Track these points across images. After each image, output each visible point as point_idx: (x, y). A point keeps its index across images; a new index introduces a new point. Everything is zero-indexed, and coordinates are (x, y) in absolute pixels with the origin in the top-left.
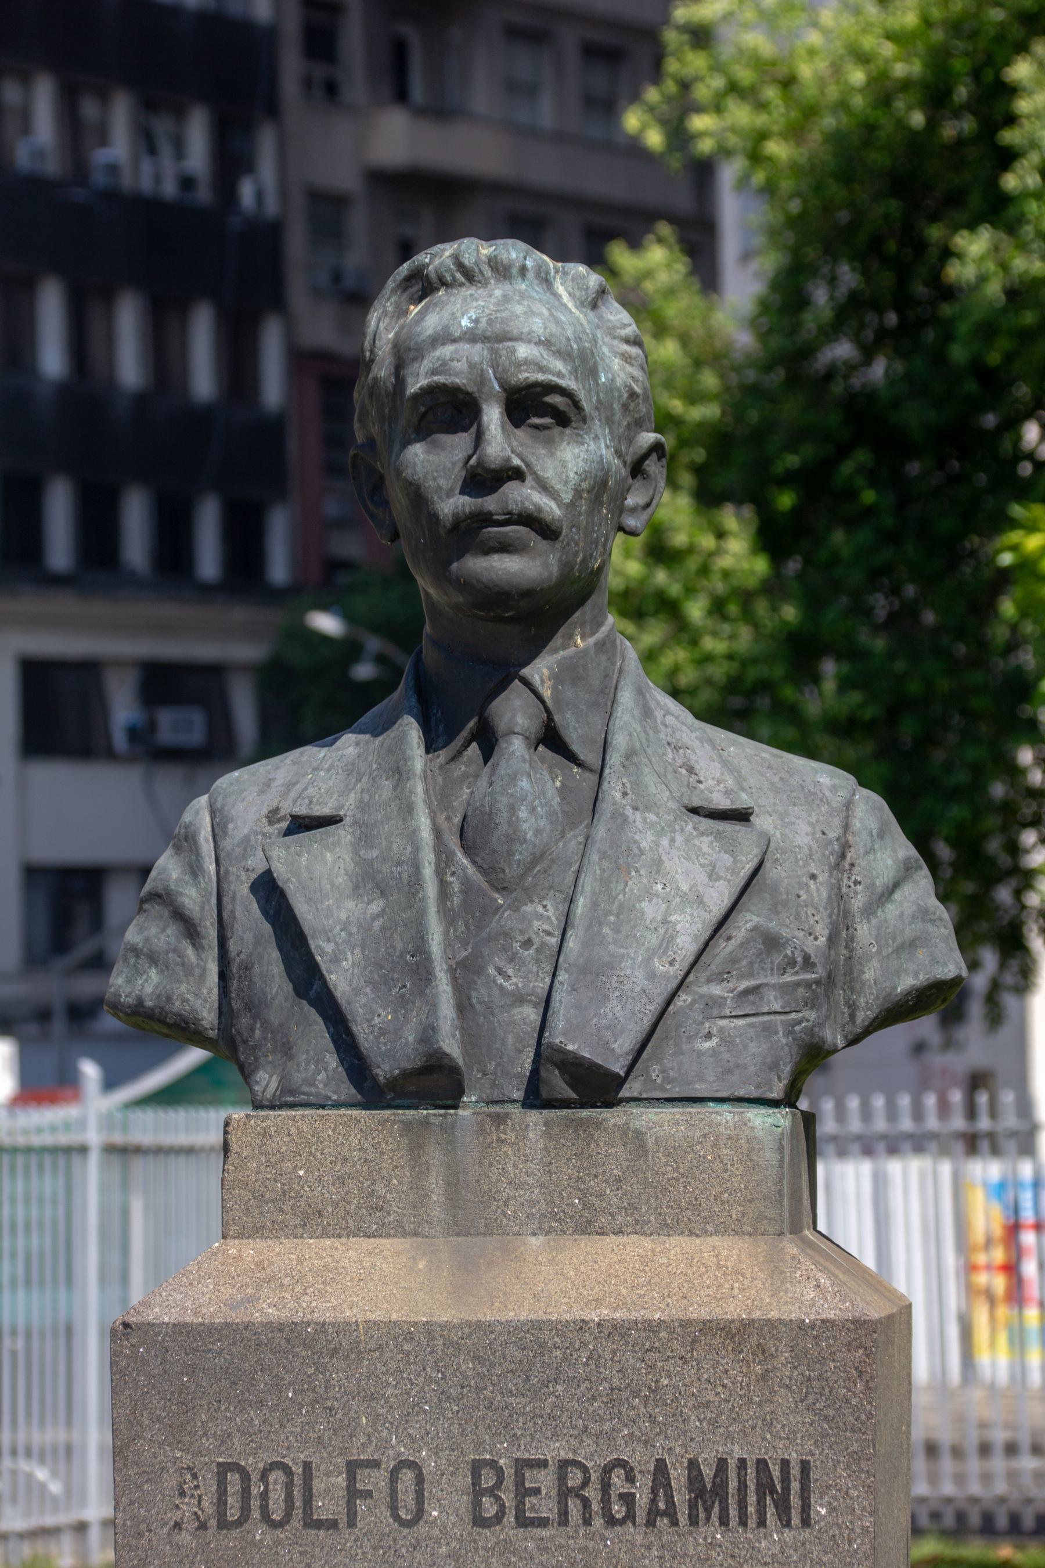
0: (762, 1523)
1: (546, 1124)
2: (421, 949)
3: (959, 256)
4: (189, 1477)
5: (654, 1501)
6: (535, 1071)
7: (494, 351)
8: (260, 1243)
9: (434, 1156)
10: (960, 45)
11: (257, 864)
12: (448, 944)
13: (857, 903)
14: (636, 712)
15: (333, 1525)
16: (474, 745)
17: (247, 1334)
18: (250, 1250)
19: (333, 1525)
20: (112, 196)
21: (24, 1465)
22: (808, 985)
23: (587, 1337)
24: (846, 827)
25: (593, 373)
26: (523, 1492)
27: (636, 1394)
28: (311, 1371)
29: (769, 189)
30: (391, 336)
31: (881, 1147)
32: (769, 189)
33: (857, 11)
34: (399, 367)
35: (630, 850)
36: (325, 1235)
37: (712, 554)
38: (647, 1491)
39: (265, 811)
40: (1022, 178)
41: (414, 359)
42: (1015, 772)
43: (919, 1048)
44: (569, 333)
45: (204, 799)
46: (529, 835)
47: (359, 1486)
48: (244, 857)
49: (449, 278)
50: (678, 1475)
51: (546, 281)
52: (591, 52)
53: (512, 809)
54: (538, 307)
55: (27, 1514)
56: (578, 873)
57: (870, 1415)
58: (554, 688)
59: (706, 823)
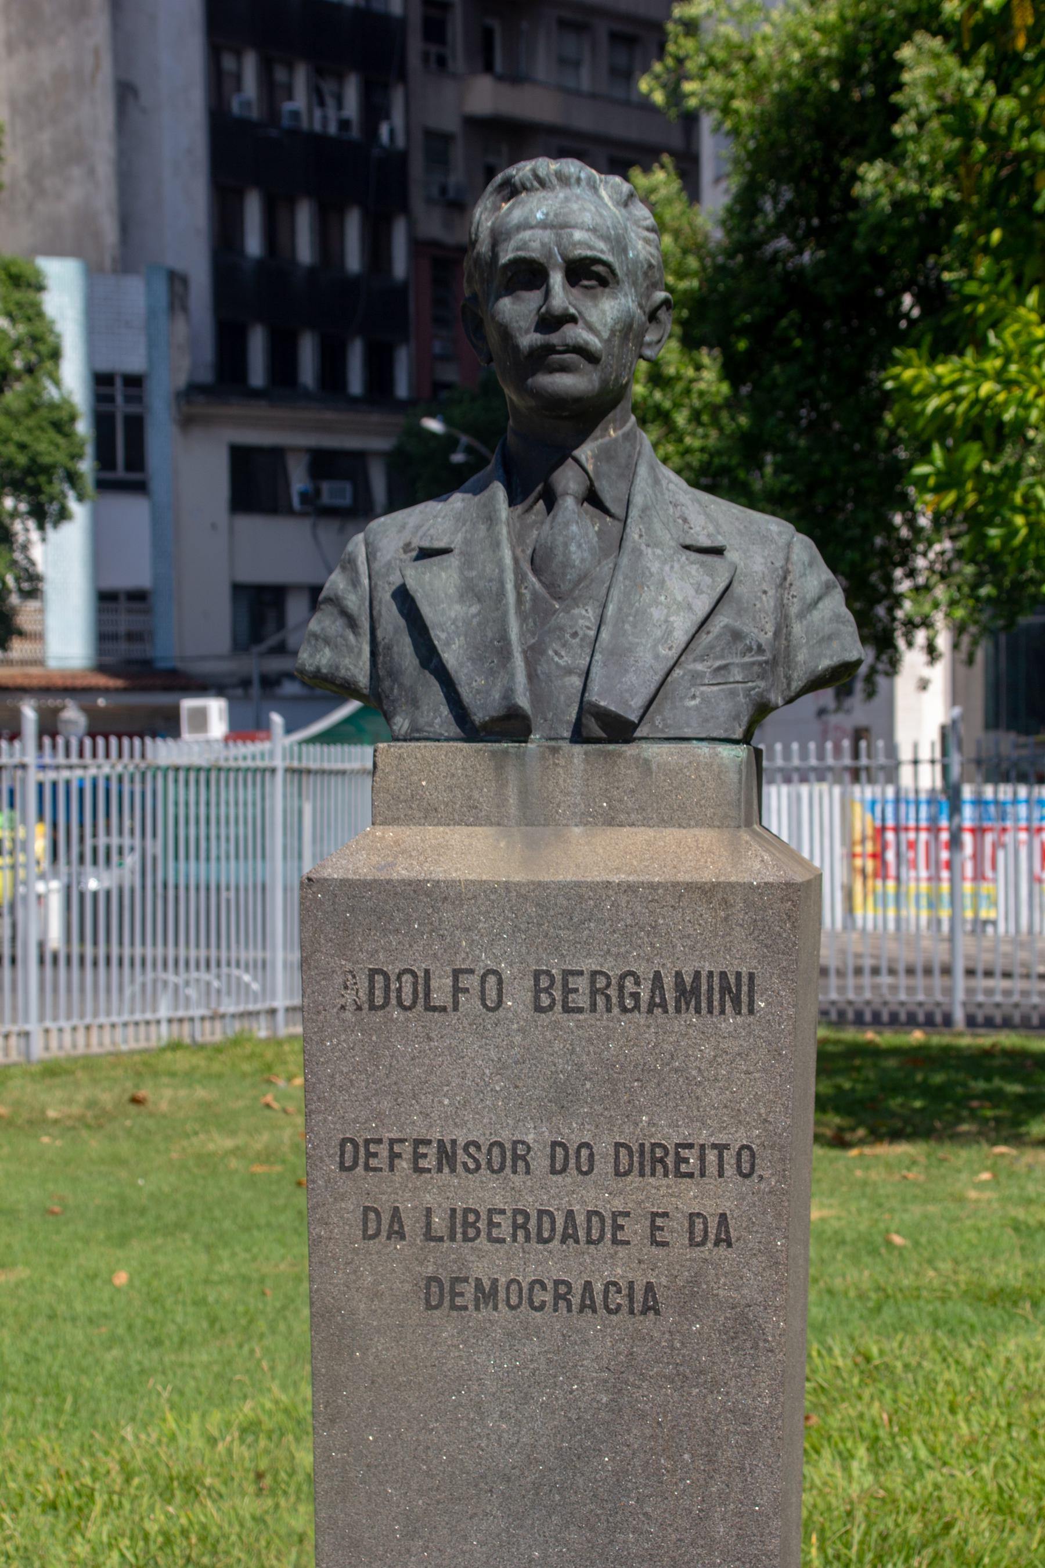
0: (722, 1012)
1: (586, 754)
2: (504, 638)
3: (862, 179)
4: (350, 977)
5: (652, 997)
6: (579, 719)
7: (558, 235)
8: (396, 829)
9: (512, 774)
10: (865, 35)
11: (396, 580)
12: (522, 634)
13: (794, 610)
14: (650, 481)
15: (444, 1009)
16: (541, 502)
17: (388, 887)
18: (390, 833)
20: (294, 133)
21: (235, 972)
22: (760, 664)
23: (611, 892)
24: (787, 559)
25: (625, 251)
26: (567, 991)
27: (642, 929)
28: (429, 911)
29: (735, 132)
30: (489, 224)
31: (795, 777)
32: (735, 132)
33: (796, 11)
34: (495, 244)
35: (643, 573)
36: (439, 824)
37: (691, 381)
38: (648, 991)
39: (401, 544)
40: (904, 126)
41: (505, 240)
42: (890, 529)
43: (822, 712)
44: (609, 223)
45: (360, 537)
46: (577, 563)
47: (461, 985)
48: (388, 575)
49: (528, 185)
50: (669, 981)
51: (594, 188)
52: (615, 37)
53: (566, 545)
54: (588, 205)
55: (238, 1003)
56: (609, 588)
57: (795, 944)
58: (595, 465)
59: (694, 556)
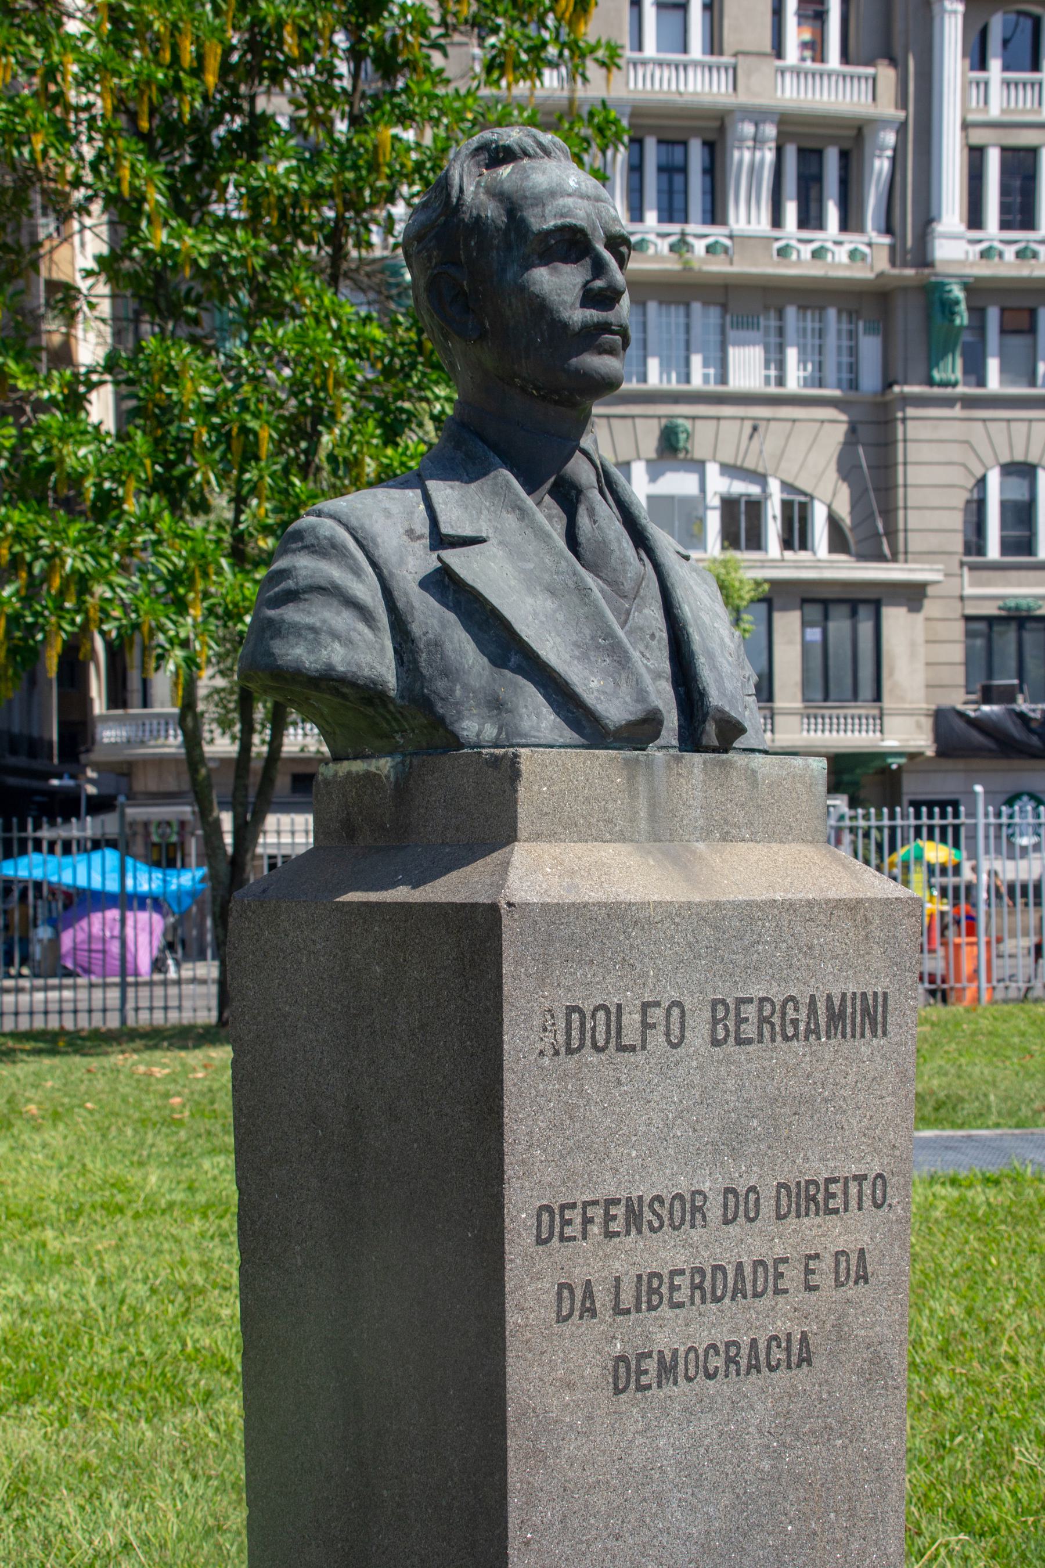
0: (863, 1036)
1: (704, 763)
17: (584, 911)
19: (633, 1049)
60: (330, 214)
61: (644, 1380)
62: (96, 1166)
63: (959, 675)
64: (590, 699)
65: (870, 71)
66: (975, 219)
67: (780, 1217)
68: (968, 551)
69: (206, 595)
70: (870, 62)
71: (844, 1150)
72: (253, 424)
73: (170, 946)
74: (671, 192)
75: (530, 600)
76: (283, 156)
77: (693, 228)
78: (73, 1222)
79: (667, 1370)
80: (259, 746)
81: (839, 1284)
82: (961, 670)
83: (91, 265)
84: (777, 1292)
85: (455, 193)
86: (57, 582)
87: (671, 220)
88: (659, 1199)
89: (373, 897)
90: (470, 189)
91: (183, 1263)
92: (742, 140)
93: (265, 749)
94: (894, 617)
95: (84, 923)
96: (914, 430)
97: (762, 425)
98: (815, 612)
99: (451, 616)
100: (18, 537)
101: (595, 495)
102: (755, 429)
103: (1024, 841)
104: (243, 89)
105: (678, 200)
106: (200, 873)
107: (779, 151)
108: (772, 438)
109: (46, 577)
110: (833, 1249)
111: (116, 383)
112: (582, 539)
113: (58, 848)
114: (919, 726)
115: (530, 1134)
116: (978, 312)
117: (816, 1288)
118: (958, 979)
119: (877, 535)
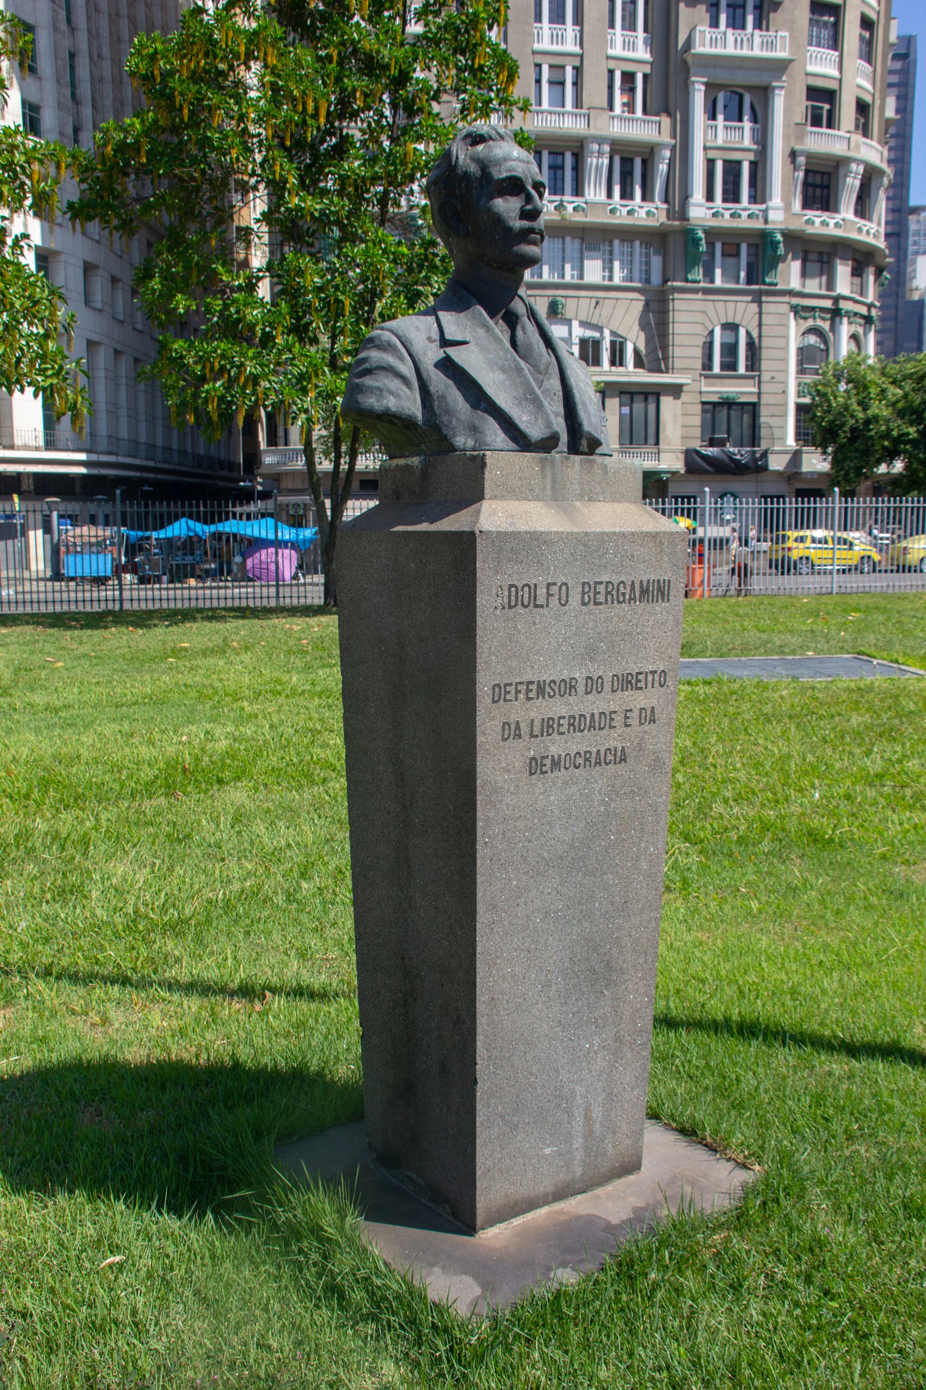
19: (542, 606)
60: (381, 188)
61: (544, 769)
62: (266, 672)
63: (698, 432)
64: (522, 426)
65: (657, 119)
66: (710, 197)
67: (613, 691)
68: (704, 368)
69: (316, 386)
70: (657, 114)
71: (646, 658)
72: (341, 297)
73: (300, 567)
74: (555, 179)
75: (491, 374)
76: (356, 158)
77: (567, 198)
78: (257, 699)
79: (556, 764)
80: (344, 467)
81: (641, 724)
82: (699, 429)
83: (259, 216)
84: (611, 727)
85: (454, 159)
86: (242, 380)
87: (555, 194)
88: (554, 681)
89: (410, 528)
90: (462, 157)
91: (310, 719)
92: (592, 153)
93: (347, 467)
94: (667, 402)
95: (257, 555)
96: (678, 305)
97: (601, 301)
98: (626, 398)
99: (451, 383)
100: (223, 356)
101: (525, 319)
102: (597, 303)
103: (728, 517)
104: (337, 124)
105: (559, 183)
106: (314, 530)
107: (611, 159)
108: (606, 307)
109: (237, 378)
110: (639, 707)
111: (272, 277)
112: (519, 343)
113: (244, 517)
114: (677, 458)
115: (490, 648)
116: (711, 245)
117: (630, 726)
118: (693, 585)
119: (658, 359)
